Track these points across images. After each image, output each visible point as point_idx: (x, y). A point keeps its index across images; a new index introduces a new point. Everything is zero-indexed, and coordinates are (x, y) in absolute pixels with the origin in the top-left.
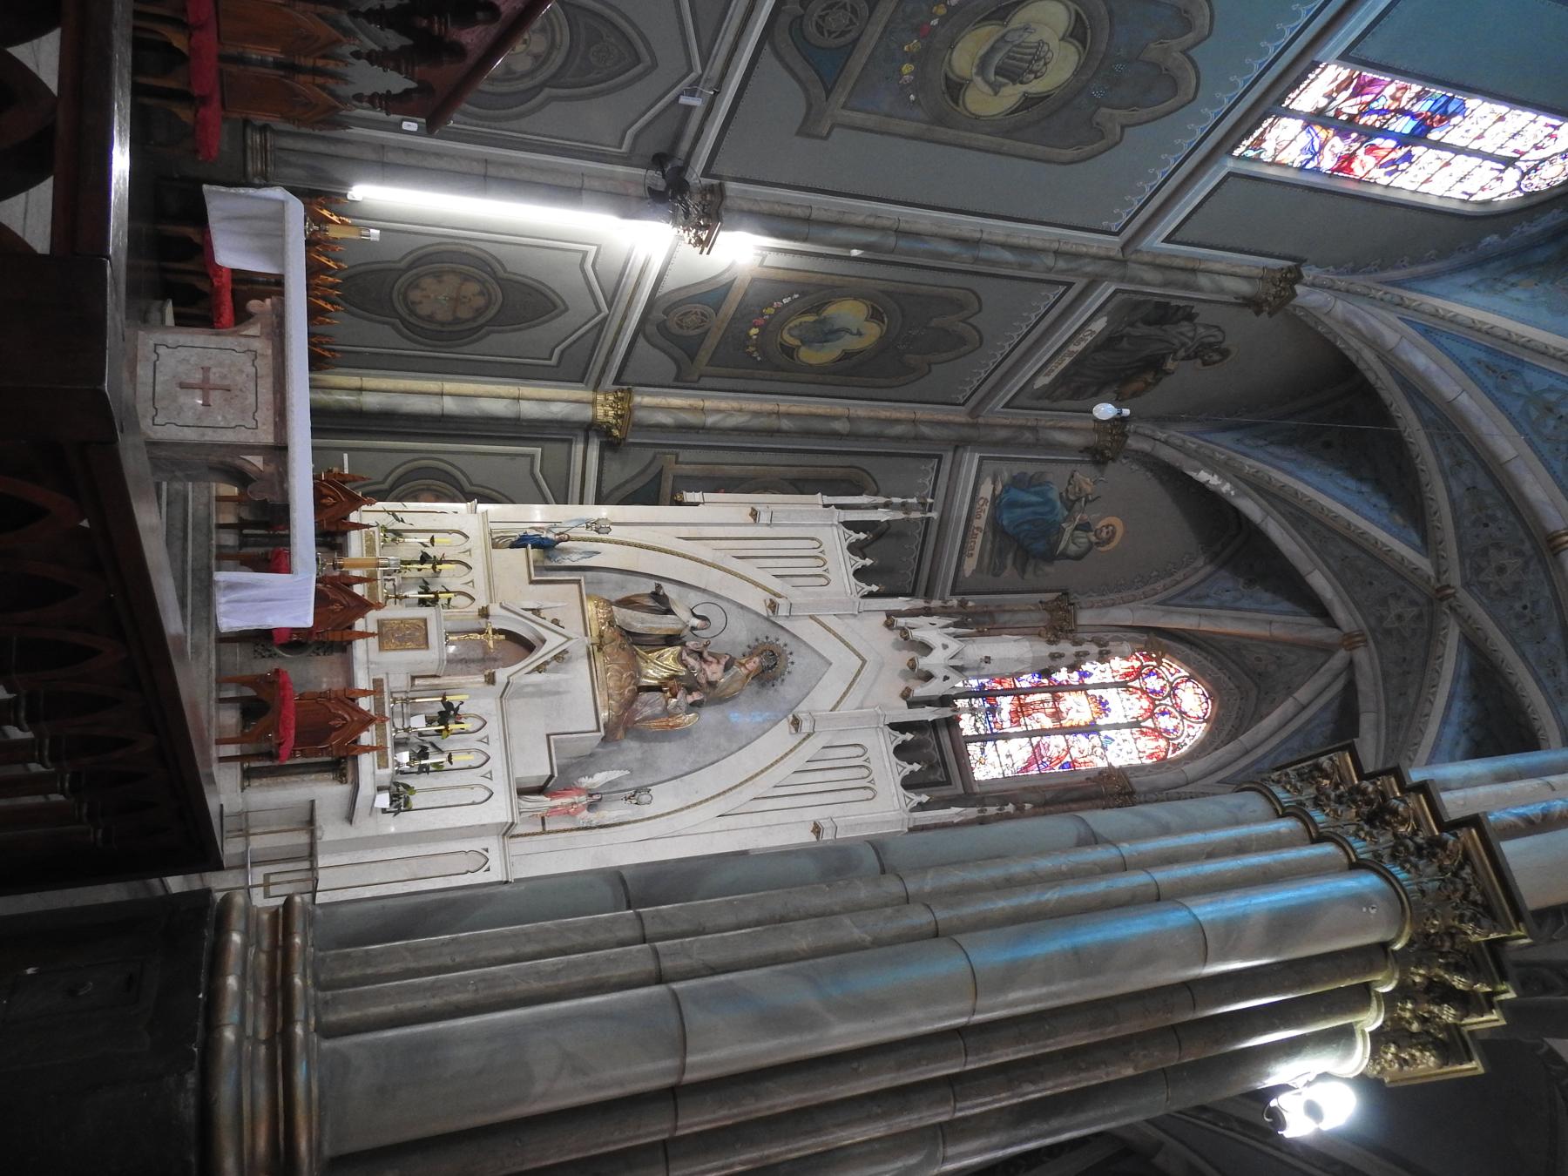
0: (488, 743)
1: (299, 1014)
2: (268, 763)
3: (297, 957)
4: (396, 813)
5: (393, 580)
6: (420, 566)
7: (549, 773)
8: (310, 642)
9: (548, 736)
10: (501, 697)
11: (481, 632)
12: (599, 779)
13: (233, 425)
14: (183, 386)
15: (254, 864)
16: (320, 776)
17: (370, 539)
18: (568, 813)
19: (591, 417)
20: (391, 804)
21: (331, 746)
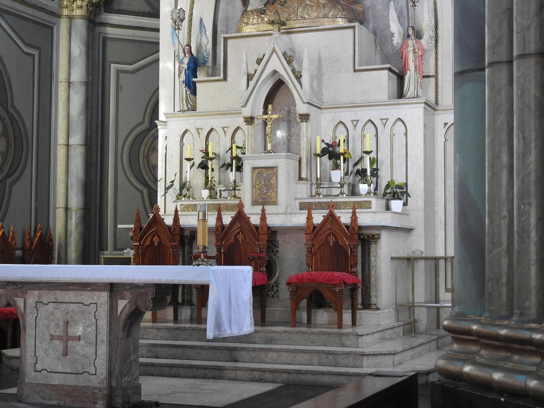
0: (358, 121)
1: (527, 335)
2: (360, 291)
3: (486, 330)
4: (408, 195)
5: (220, 191)
6: (210, 170)
7: (386, 72)
8: (267, 258)
9: (355, 71)
10: (320, 108)
11: (265, 124)
12: (395, 27)
13: (94, 320)
14: (65, 353)
15: (437, 301)
16: (372, 254)
17: (187, 208)
18: (422, 56)
19: (84, 21)
20: (400, 199)
21: (349, 245)
